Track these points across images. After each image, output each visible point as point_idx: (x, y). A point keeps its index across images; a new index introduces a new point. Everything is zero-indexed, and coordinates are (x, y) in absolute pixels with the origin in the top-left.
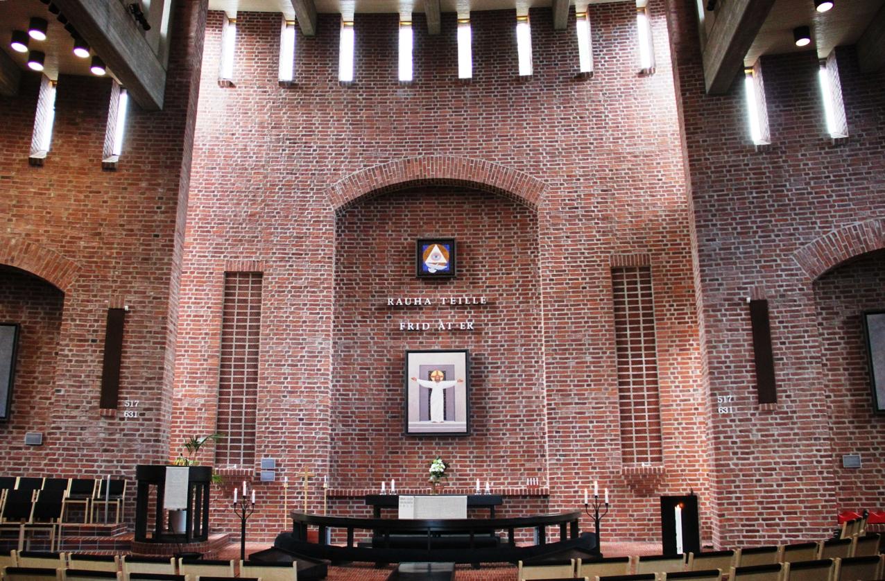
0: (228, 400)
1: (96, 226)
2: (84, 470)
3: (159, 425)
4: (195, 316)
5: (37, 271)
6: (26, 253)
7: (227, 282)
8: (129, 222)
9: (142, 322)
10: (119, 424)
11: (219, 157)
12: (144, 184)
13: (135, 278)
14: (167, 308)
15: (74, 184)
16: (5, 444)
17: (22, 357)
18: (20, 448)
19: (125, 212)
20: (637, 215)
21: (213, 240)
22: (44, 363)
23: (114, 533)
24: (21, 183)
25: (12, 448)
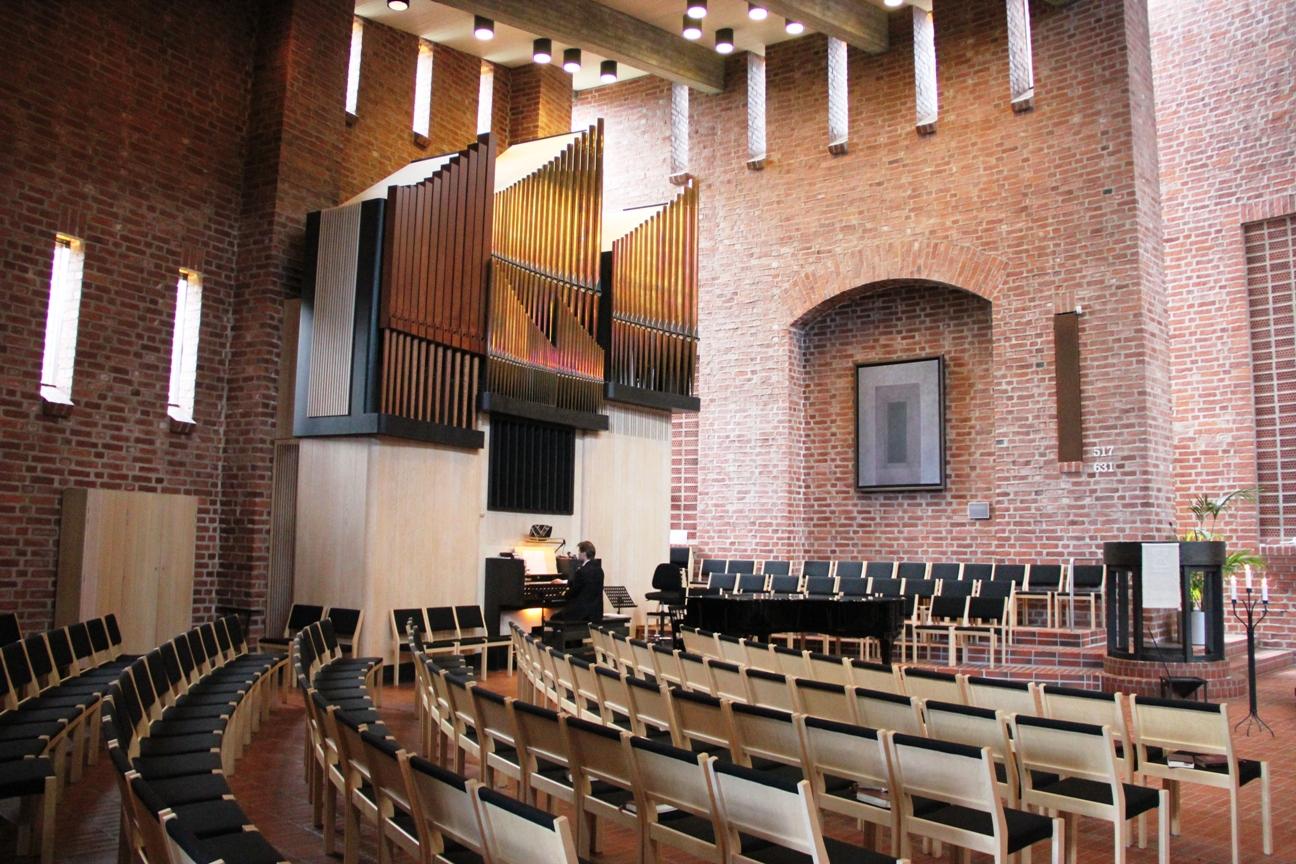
0: (1273, 433)
1: (1020, 197)
2: (1045, 551)
3: (1148, 481)
4: (1201, 305)
5: (951, 279)
6: (933, 258)
7: (1247, 240)
8: (1065, 181)
9: (1105, 326)
10: (1088, 483)
11: (1202, 40)
12: (1076, 119)
13: (1085, 262)
14: (1139, 299)
15: (979, 146)
16: (943, 520)
17: (952, 401)
18: (963, 525)
19: (1057, 167)
20: (282, 199)
21: (1215, 177)
22: (981, 405)
23: (1084, 644)
24: (913, 164)
25: (953, 525)
